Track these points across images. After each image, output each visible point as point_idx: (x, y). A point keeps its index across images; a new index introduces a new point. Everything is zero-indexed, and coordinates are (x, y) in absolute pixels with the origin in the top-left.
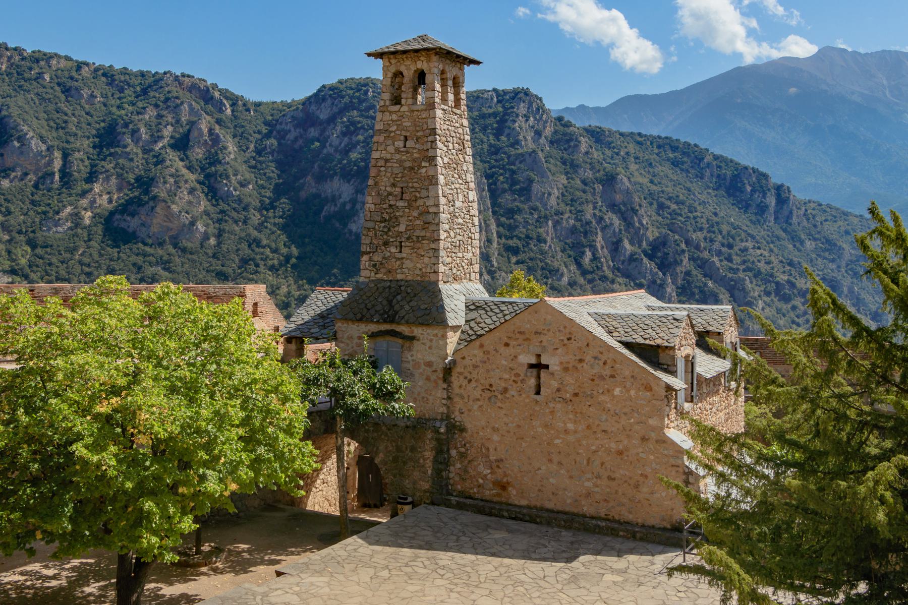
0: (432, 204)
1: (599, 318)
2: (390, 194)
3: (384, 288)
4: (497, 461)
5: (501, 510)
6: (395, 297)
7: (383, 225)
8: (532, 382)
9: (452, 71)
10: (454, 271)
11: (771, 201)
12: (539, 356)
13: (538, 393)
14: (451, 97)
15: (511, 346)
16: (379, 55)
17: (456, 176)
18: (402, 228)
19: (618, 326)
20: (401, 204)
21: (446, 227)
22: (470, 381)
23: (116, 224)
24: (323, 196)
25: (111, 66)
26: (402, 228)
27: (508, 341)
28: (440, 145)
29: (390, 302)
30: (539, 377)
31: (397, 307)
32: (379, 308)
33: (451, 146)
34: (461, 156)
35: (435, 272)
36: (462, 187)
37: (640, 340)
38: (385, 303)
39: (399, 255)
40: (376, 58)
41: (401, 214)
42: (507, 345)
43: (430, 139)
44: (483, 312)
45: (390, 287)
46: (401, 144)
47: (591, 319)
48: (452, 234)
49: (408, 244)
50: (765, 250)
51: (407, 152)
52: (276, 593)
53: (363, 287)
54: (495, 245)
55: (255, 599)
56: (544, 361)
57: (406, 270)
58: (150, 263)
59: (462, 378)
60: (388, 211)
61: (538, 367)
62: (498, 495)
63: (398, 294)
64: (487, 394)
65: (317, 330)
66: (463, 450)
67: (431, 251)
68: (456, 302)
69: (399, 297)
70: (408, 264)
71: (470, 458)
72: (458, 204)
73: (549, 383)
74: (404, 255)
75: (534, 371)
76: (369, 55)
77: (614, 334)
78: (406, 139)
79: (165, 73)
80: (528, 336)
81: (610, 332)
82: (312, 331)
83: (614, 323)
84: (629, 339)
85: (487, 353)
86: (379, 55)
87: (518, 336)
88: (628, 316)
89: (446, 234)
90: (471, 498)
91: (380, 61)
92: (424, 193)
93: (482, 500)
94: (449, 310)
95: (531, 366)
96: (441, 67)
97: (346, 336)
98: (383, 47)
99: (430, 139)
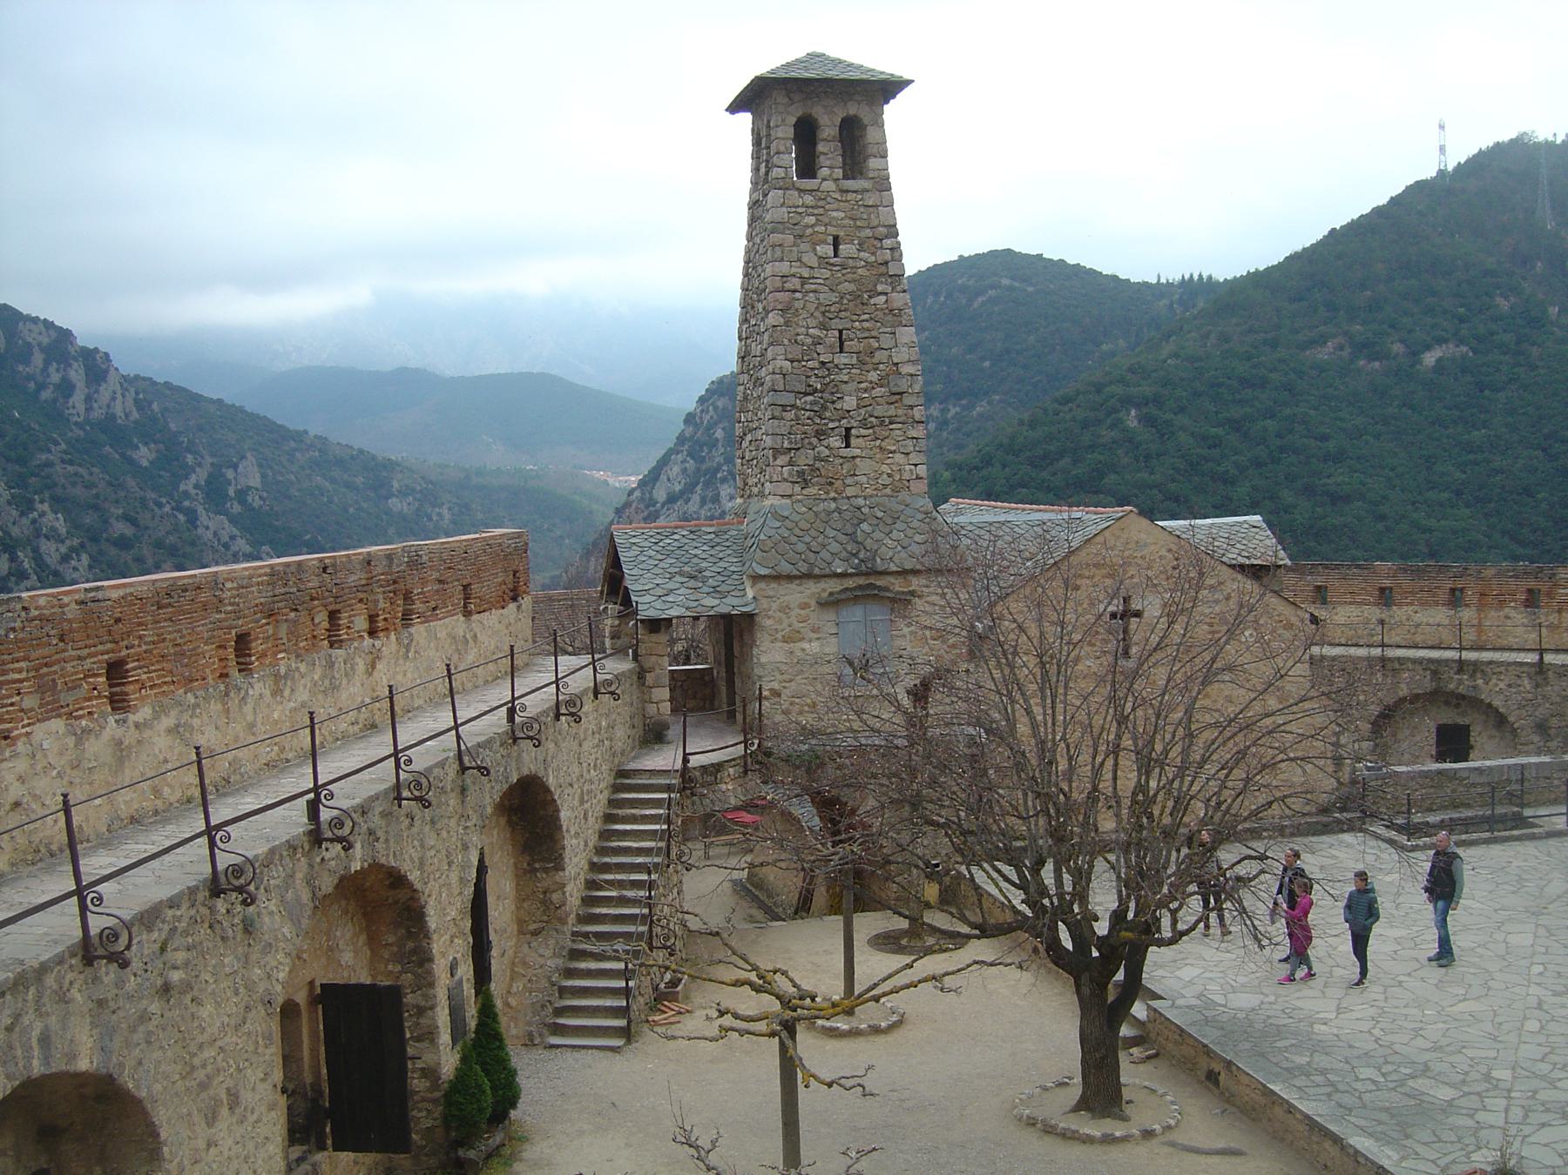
2: (818, 342)
7: (810, 398)
11: (77, 374)
18: (850, 402)
20: (842, 359)
29: (852, 536)
32: (835, 547)
41: (846, 378)
46: (830, 250)
50: (80, 465)
51: (844, 266)
56: (1136, 605)
67: (909, 442)
70: (864, 466)
78: (836, 242)
92: (886, 341)
97: (775, 606)
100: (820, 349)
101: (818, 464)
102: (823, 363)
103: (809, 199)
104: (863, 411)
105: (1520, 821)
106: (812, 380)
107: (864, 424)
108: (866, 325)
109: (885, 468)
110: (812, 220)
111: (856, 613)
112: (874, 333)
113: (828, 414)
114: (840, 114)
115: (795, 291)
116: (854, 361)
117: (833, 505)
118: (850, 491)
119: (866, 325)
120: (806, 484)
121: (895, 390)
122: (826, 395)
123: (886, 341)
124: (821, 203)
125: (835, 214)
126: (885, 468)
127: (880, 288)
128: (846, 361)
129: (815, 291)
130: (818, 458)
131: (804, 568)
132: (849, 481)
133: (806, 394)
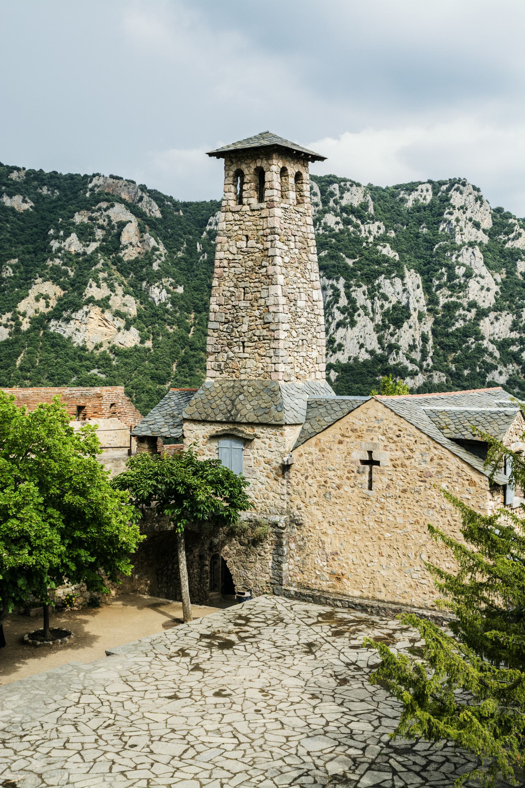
0: (273, 302)
1: (433, 415)
3: (228, 388)
4: (332, 554)
5: (334, 600)
6: (237, 396)
7: (226, 325)
8: (365, 478)
9: (292, 170)
10: (297, 370)
12: (370, 453)
13: (370, 488)
14: (292, 195)
15: (345, 443)
16: (218, 154)
17: (299, 275)
18: (245, 328)
19: (451, 422)
21: (286, 326)
22: (307, 478)
23: (52, 330)
24: (138, 301)
25: (41, 171)
26: (245, 328)
27: (342, 439)
28: (279, 244)
29: (233, 401)
30: (371, 473)
31: (239, 407)
33: (292, 245)
34: (304, 255)
35: (276, 371)
36: (305, 286)
37: (469, 437)
38: (228, 402)
39: (242, 355)
40: (218, 158)
41: (244, 314)
42: (340, 442)
43: (270, 238)
44: (324, 410)
45: (233, 387)
47: (425, 417)
48: (294, 334)
49: (250, 344)
52: (99, 670)
53: (208, 387)
54: (431, 342)
55: (78, 675)
57: (248, 370)
58: (87, 367)
59: (299, 475)
60: (232, 311)
61: (371, 462)
62: (334, 587)
63: (241, 393)
64: (322, 491)
65: (167, 429)
66: (302, 543)
67: (272, 351)
68: (297, 401)
69: (241, 397)
71: (308, 551)
72: (300, 303)
73: (381, 481)
74: (247, 355)
75: (367, 467)
76: (211, 155)
77: (445, 431)
79: (94, 176)
80: (359, 434)
81: (441, 429)
82: (162, 430)
83: (447, 420)
84: (458, 436)
85: (321, 450)
86: (218, 154)
87: (351, 433)
88: (462, 413)
89: (286, 334)
90: (308, 588)
91: (222, 160)
92: (264, 294)
93: (319, 591)
94: (287, 408)
95: (364, 462)
96: (281, 165)
98: (230, 143)
99: (270, 238)
100: (233, 298)
101: (228, 361)
102: (234, 306)
103: (237, 217)
104: (250, 333)
105: (62, 634)
106: (228, 316)
107: (250, 340)
108: (257, 284)
109: (260, 365)
110: (237, 228)
111: (225, 443)
112: (260, 289)
113: (233, 334)
114: (253, 167)
115: (224, 267)
116: (248, 305)
117: (232, 384)
118: (243, 377)
119: (257, 284)
120: (221, 371)
121: (266, 321)
122: (234, 324)
123: (264, 294)
124: (242, 218)
125: (247, 223)
126: (260, 365)
127: (264, 263)
128: (244, 305)
129: (234, 267)
130: (228, 358)
131: (203, 417)
132: (243, 371)
133: (225, 323)
